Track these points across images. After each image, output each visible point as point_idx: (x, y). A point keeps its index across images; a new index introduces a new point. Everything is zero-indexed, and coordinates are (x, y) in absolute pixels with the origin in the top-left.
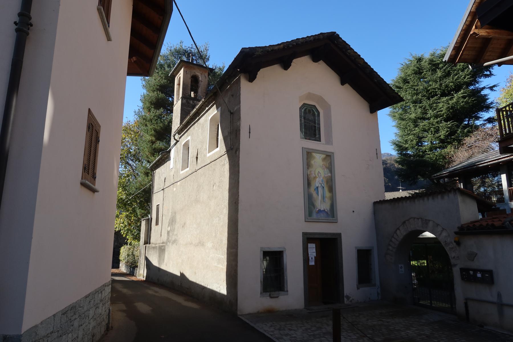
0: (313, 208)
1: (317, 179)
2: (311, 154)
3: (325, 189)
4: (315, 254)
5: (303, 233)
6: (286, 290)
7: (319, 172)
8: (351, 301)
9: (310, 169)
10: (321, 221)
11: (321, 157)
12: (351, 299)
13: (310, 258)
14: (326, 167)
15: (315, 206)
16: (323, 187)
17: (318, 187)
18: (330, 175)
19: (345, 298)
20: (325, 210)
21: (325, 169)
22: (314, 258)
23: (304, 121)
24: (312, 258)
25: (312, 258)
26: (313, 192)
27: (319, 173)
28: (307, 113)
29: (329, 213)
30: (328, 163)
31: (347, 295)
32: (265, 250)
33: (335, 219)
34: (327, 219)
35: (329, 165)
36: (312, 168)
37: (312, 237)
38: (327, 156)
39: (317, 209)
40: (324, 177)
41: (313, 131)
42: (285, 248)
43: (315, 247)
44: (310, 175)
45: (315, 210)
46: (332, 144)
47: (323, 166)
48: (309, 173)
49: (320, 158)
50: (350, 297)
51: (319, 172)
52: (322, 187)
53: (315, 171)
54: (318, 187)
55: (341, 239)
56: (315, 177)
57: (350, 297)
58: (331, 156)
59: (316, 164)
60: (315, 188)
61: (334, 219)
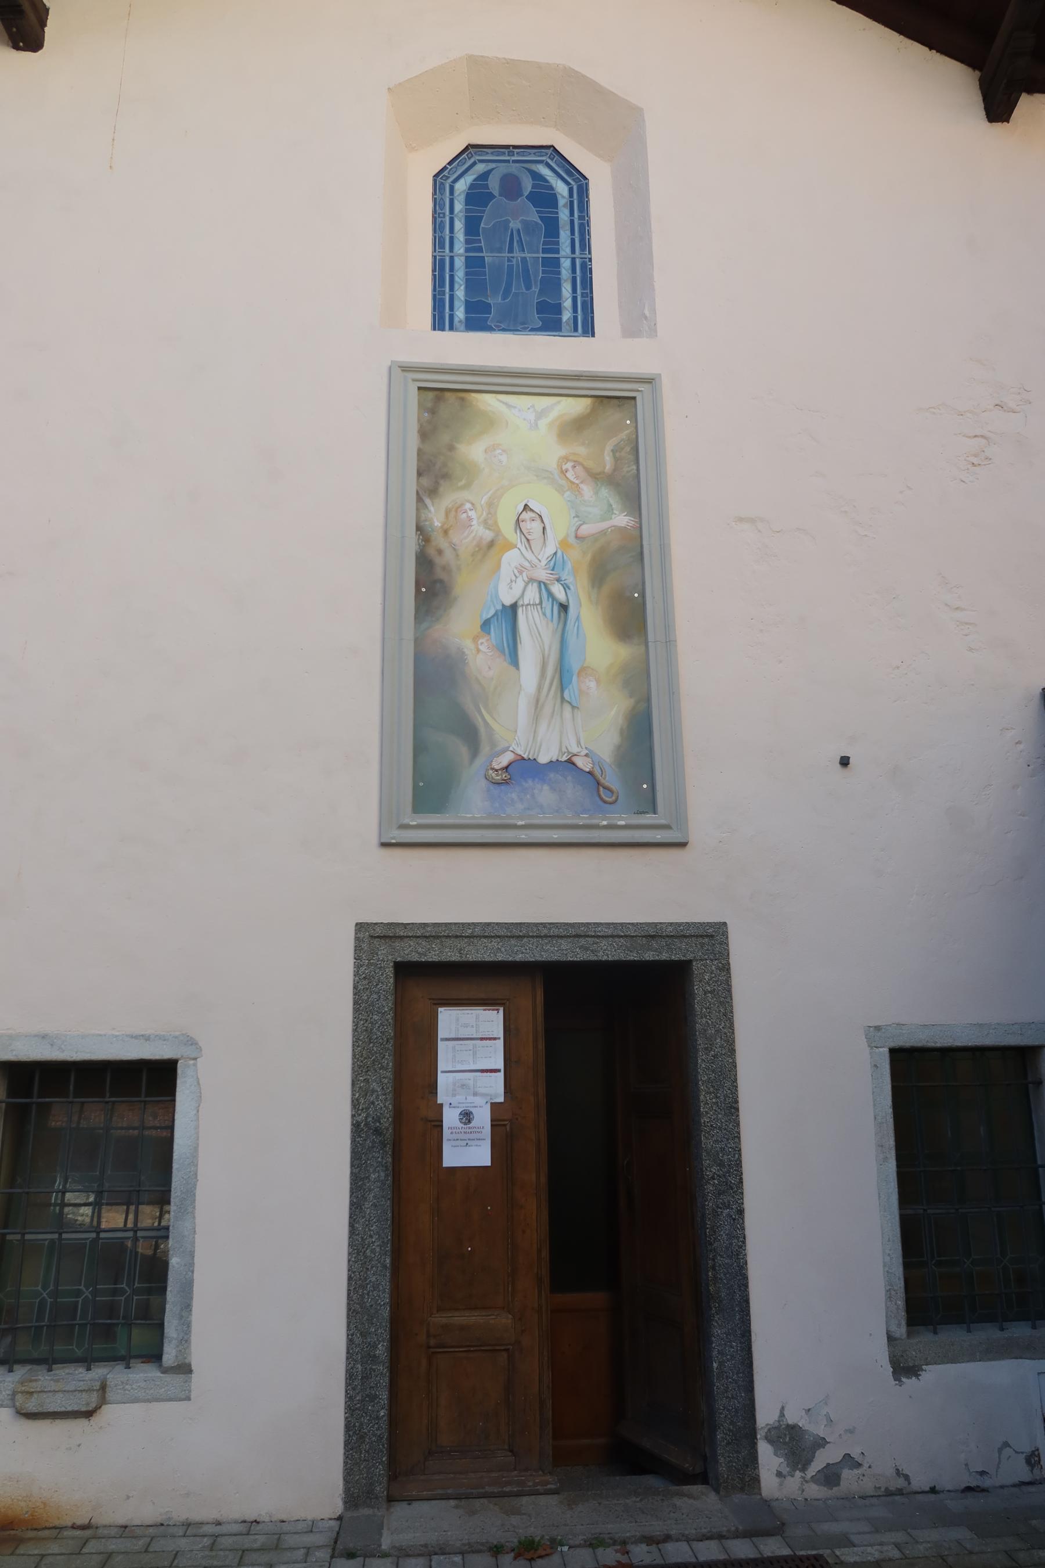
0: (464, 751)
1: (511, 559)
2: (463, 399)
3: (578, 618)
4: (495, 1087)
5: (360, 927)
6: (169, 1356)
7: (526, 507)
8: (830, 1477)
9: (449, 498)
10: (523, 836)
11: (553, 414)
12: (821, 1460)
13: (450, 1118)
14: (596, 477)
15: (482, 730)
16: (564, 608)
17: (514, 607)
18: (622, 520)
19: (765, 1450)
20: (576, 760)
21: (587, 490)
22: (483, 1118)
23: (467, 242)
24: (467, 1116)
25: (467, 1116)
26: (468, 645)
27: (526, 515)
28: (491, 196)
29: (611, 779)
30: (609, 448)
31: (791, 1418)
32: (179, 1065)
33: (663, 822)
34: (584, 819)
35: (617, 460)
36: (467, 486)
37: (450, 955)
38: (603, 400)
39: (499, 754)
40: (572, 540)
41: (535, 289)
42: (191, 1042)
43: (498, 1030)
44: (446, 532)
45: (480, 761)
46: (653, 332)
47: (564, 472)
48: (437, 524)
49: (543, 423)
50: (821, 1443)
51: (526, 507)
52: (547, 604)
53: (492, 505)
54: (514, 607)
55: (726, 969)
56: (491, 544)
57: (821, 1443)
58: (634, 398)
59: (504, 458)
60: (492, 612)
61: (648, 819)
